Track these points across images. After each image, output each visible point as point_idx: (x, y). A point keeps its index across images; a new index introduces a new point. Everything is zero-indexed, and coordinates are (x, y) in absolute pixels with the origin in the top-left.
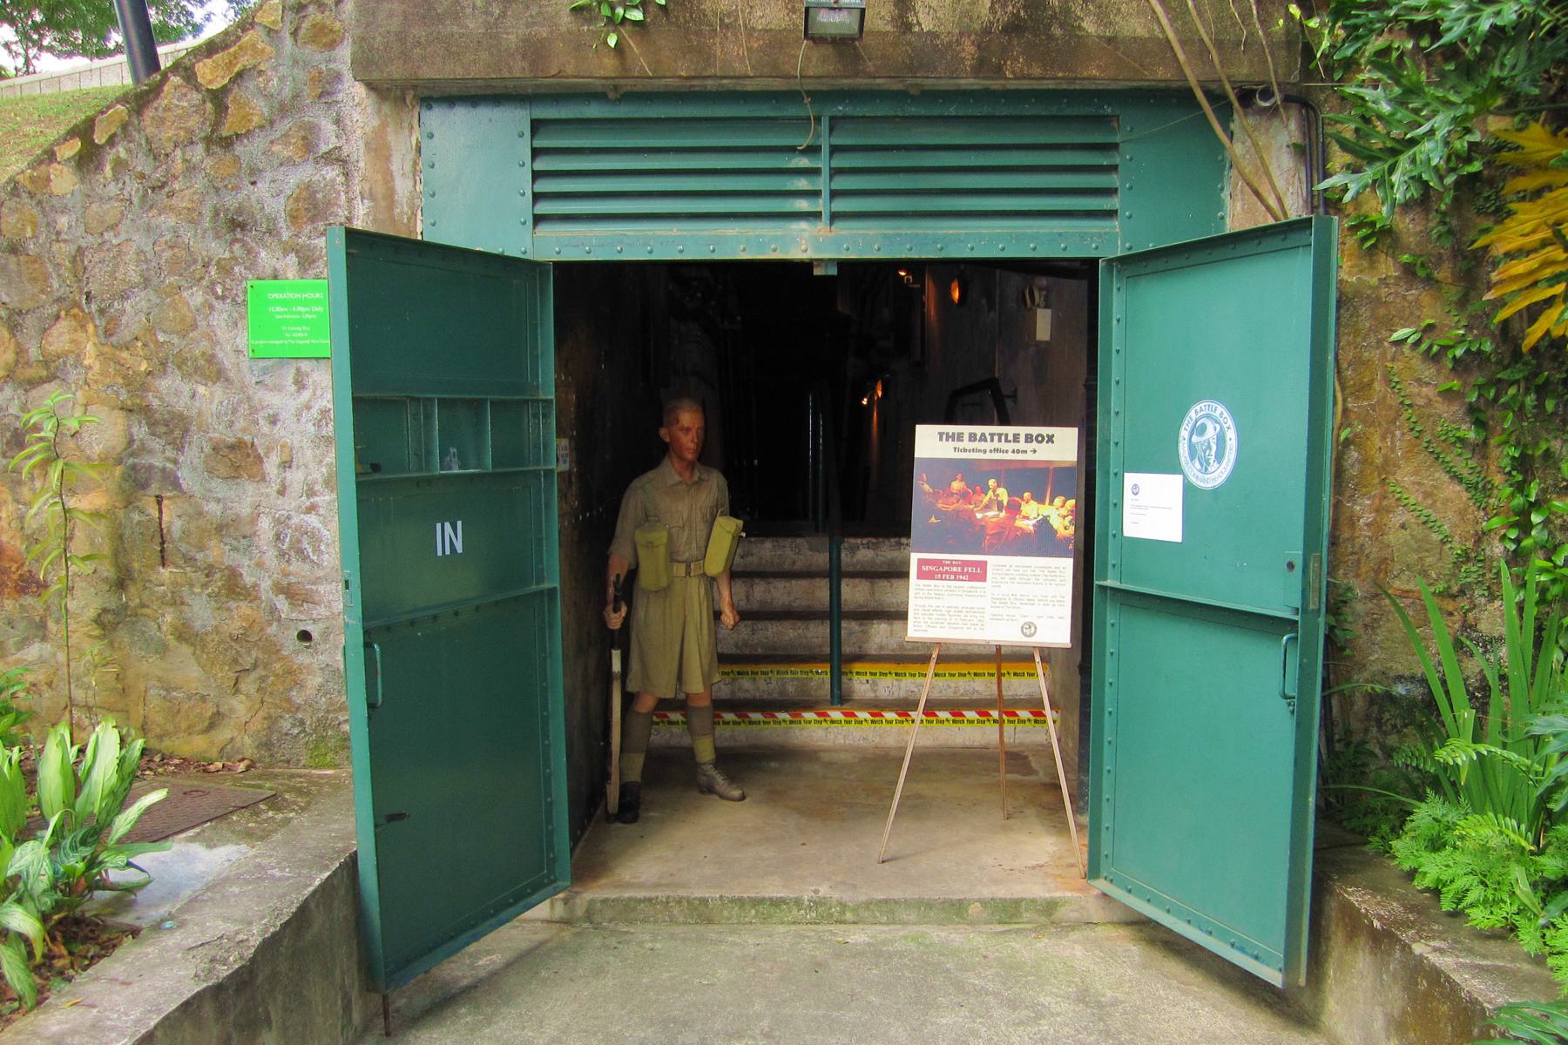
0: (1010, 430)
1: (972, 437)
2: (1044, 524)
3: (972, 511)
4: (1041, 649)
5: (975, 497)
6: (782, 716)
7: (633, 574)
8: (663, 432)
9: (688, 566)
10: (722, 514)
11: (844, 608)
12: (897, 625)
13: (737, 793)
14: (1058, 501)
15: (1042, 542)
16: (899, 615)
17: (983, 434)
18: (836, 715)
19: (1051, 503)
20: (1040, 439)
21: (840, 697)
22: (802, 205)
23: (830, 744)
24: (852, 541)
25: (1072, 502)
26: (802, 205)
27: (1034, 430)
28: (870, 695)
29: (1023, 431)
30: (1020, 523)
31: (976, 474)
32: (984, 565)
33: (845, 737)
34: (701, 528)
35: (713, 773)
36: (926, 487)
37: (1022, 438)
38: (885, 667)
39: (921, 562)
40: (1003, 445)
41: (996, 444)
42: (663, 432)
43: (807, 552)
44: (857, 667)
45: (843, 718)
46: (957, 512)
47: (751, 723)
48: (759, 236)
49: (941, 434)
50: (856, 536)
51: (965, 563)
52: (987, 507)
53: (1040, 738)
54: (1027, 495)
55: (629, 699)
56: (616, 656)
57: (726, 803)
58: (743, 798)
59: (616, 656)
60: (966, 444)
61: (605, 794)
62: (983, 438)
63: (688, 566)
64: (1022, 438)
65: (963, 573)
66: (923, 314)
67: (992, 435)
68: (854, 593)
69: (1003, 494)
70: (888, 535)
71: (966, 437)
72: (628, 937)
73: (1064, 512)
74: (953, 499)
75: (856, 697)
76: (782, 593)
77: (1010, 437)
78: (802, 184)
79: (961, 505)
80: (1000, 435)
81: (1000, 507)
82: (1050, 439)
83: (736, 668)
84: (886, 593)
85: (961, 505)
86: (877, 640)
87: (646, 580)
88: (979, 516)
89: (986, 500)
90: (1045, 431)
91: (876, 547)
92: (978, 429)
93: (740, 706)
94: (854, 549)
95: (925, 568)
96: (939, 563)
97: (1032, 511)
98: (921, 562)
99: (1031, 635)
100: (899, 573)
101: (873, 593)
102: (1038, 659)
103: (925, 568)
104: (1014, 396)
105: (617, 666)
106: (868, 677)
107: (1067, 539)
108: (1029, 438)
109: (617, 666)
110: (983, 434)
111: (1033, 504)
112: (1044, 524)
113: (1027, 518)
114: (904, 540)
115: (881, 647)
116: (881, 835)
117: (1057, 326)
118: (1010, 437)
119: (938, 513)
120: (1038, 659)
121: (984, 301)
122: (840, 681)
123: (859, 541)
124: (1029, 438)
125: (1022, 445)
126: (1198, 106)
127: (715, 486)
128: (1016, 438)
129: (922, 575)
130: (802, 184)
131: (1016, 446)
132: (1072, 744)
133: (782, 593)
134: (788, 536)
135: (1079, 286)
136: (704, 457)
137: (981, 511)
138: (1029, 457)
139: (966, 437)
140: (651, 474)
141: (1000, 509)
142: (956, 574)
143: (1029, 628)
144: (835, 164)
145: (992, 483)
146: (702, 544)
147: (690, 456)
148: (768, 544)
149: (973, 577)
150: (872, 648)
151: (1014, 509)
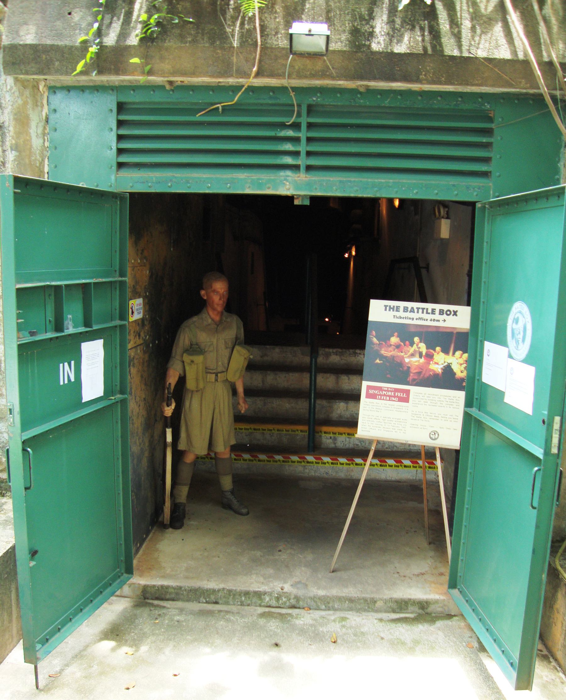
0: (429, 306)
1: (406, 309)
2: (448, 369)
3: (403, 357)
4: (441, 449)
5: (405, 348)
6: (278, 457)
7: (182, 380)
8: (203, 292)
9: (217, 375)
10: (240, 344)
11: (317, 428)
12: (351, 404)
13: (244, 511)
14: (458, 353)
15: (446, 380)
16: (353, 423)
17: (412, 308)
18: (310, 458)
19: (454, 354)
20: (448, 313)
21: (314, 447)
22: (288, 160)
23: (306, 475)
24: (327, 350)
25: (466, 356)
26: (288, 160)
27: (445, 307)
28: (332, 446)
29: (438, 307)
30: (433, 367)
31: (407, 334)
32: (408, 392)
33: (315, 471)
34: (227, 353)
35: (232, 497)
36: (375, 340)
37: (437, 312)
38: (341, 429)
39: (369, 387)
40: (425, 316)
41: (420, 315)
42: (203, 292)
43: (298, 355)
44: (325, 429)
45: (314, 460)
46: (393, 357)
47: (259, 461)
48: (259, 179)
49: (386, 306)
50: (329, 347)
51: (396, 390)
52: (413, 355)
53: (430, 477)
54: (438, 349)
55: (178, 456)
56: (169, 432)
57: (237, 515)
58: (248, 514)
59: (169, 432)
60: (401, 313)
61: (163, 511)
62: (412, 310)
63: (217, 375)
64: (437, 312)
65: (395, 397)
66: (379, 210)
67: (418, 309)
68: (326, 382)
69: (423, 347)
70: (348, 348)
71: (401, 309)
72: (164, 611)
73: (461, 361)
74: (390, 349)
75: (323, 446)
76: (283, 380)
77: (430, 311)
78: (289, 147)
79: (395, 353)
80: (423, 309)
81: (421, 355)
82: (455, 313)
83: (253, 426)
84: (346, 383)
85: (395, 353)
86: (339, 412)
87: (190, 384)
88: (407, 360)
89: (412, 350)
90: (452, 308)
91: (341, 354)
92: (409, 305)
93: (254, 449)
94: (328, 355)
95: (371, 392)
96: (380, 389)
97: (440, 360)
98: (369, 387)
99: (435, 439)
100: (356, 397)
101: (337, 383)
102: (438, 455)
103: (371, 392)
104: (427, 268)
105: (169, 439)
106: (332, 435)
107: (462, 380)
108: (441, 312)
109: (169, 439)
110: (412, 308)
111: (442, 354)
112: (448, 369)
113: (437, 364)
114: (358, 351)
115: (340, 416)
116: (332, 556)
117: (453, 230)
118: (430, 311)
119: (382, 357)
120: (438, 455)
121: (412, 208)
122: (314, 436)
123: (331, 350)
124: (441, 312)
125: (437, 316)
126: (546, 106)
127: (234, 328)
128: (433, 311)
129: (368, 396)
130: (289, 147)
131: (433, 317)
132: (449, 484)
133: (283, 380)
134: (290, 345)
135: (470, 208)
136: (229, 308)
137: (409, 357)
138: (441, 324)
139: (401, 309)
140: (195, 319)
141: (421, 356)
142: (390, 396)
143: (434, 435)
144: (311, 134)
145: (416, 339)
146: (226, 361)
147: (219, 309)
148: (277, 350)
149: (401, 400)
150: (334, 416)
151: (429, 357)
